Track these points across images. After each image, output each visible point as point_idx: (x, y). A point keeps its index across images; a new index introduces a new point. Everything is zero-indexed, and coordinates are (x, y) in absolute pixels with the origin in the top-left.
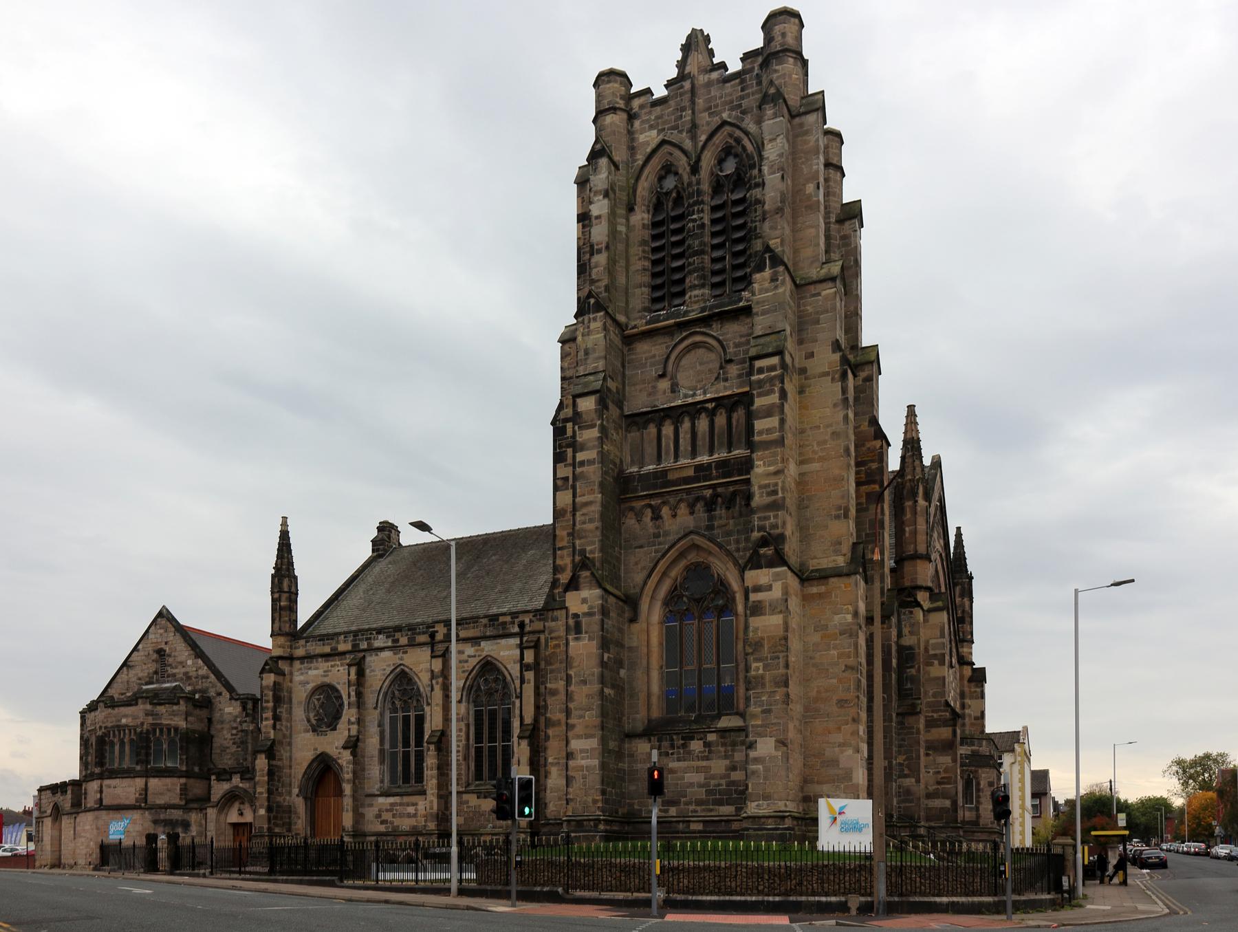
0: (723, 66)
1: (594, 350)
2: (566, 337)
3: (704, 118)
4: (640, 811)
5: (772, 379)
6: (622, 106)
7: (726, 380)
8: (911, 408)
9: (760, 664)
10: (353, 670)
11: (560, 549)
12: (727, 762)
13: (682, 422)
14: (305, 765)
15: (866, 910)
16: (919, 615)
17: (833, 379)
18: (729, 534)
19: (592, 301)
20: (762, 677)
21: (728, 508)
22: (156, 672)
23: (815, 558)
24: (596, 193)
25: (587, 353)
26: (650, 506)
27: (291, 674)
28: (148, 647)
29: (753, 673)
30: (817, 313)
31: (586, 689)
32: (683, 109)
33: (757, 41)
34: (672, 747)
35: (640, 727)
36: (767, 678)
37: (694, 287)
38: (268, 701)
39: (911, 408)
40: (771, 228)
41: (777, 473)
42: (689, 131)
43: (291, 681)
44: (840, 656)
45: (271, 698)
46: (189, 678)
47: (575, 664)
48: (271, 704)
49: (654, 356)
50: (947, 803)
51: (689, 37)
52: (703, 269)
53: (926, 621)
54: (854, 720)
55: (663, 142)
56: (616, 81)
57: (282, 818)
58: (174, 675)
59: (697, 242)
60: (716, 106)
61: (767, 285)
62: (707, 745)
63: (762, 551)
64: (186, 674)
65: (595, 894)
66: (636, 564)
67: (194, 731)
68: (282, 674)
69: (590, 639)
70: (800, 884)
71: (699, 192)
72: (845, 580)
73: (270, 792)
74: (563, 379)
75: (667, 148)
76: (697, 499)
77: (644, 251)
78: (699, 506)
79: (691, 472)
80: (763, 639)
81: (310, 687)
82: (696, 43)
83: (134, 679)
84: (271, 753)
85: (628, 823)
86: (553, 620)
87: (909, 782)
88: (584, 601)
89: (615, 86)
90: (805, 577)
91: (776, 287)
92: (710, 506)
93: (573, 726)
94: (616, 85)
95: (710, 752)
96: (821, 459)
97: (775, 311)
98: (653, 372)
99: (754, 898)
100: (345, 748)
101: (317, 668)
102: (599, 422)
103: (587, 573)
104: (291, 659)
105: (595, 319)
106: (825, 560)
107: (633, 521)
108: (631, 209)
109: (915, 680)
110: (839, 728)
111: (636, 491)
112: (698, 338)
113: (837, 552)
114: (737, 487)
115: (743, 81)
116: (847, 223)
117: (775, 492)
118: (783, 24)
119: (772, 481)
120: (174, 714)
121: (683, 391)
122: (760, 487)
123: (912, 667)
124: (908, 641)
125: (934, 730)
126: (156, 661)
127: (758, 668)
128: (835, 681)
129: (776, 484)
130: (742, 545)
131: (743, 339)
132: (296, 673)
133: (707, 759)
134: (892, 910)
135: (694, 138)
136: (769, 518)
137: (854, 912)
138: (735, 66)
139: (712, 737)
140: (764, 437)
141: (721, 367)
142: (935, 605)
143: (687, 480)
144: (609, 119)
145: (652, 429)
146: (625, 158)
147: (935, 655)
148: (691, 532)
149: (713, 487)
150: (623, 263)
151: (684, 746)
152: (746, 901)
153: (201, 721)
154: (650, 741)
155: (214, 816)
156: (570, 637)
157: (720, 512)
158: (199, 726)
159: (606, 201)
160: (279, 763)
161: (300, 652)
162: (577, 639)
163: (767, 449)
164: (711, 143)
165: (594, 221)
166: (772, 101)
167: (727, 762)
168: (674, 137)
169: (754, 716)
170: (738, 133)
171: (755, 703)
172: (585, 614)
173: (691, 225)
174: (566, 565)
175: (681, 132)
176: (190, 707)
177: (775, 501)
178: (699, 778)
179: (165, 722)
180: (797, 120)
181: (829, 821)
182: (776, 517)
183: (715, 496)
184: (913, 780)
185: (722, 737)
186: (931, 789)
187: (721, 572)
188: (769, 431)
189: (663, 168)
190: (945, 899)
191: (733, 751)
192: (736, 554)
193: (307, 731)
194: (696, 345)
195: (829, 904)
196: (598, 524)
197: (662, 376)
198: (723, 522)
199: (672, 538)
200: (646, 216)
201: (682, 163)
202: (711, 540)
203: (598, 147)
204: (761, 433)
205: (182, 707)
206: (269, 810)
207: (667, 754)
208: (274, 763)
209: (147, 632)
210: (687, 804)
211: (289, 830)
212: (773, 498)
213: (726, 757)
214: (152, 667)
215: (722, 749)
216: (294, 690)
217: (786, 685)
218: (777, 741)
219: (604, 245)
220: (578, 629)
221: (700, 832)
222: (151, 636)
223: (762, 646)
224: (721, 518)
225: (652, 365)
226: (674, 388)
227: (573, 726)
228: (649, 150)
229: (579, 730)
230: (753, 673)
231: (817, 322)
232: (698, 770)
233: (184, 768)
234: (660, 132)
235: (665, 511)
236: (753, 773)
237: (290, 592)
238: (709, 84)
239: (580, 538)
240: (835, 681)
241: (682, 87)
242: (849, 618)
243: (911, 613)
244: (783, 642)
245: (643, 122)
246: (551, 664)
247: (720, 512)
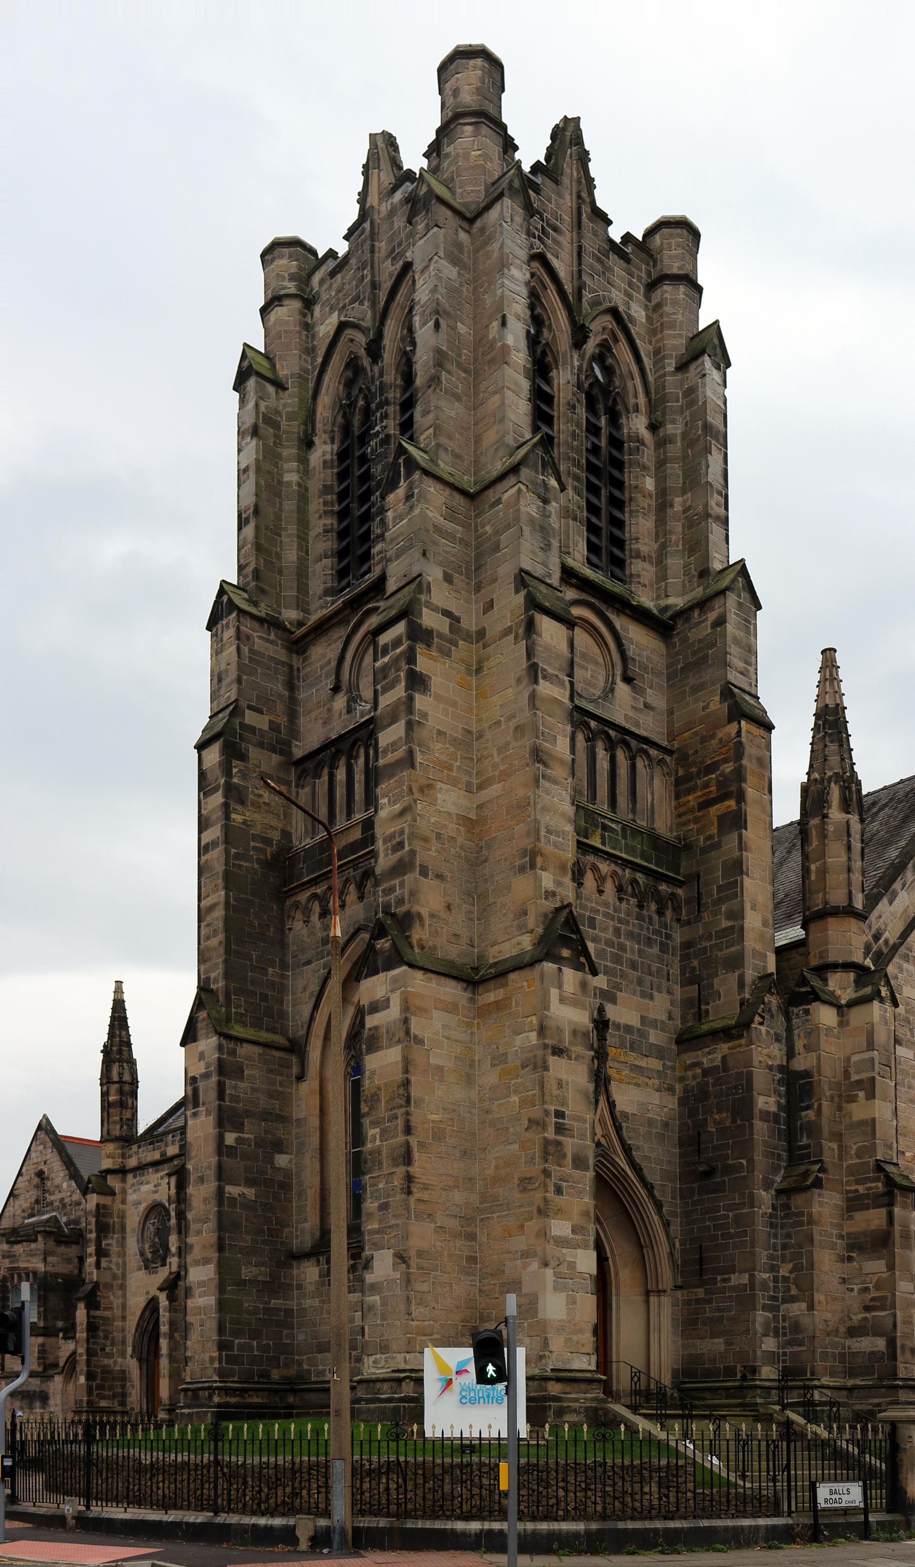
4: (309, 1371)
8: (829, 655)
10: (173, 1180)
14: (139, 1313)
15: (321, 1542)
16: (826, 1016)
17: (516, 638)
22: (37, 1201)
23: (495, 943)
26: (315, 896)
27: (124, 1192)
28: (30, 1170)
38: (91, 1232)
39: (829, 655)
43: (124, 1202)
44: (523, 1102)
45: (93, 1227)
46: (64, 1206)
48: (93, 1236)
50: (880, 1344)
53: (842, 1024)
54: (539, 1211)
55: (342, 326)
56: (281, 257)
57: (111, 1388)
58: (51, 1203)
64: (62, 1200)
66: (305, 989)
67: (56, 1275)
68: (112, 1193)
69: (208, 1114)
70: (295, 1494)
72: (526, 973)
73: (90, 1353)
77: (325, 503)
81: (142, 1207)
82: (384, 148)
83: (19, 1212)
84: (92, 1303)
85: (294, 1391)
87: (797, 1309)
90: (474, 977)
94: (283, 262)
100: (161, 1289)
101: (148, 1183)
104: (122, 1172)
106: (506, 946)
108: (308, 443)
109: (813, 1129)
110: (522, 1227)
111: (301, 875)
113: (523, 929)
116: (692, 367)
120: (32, 1254)
123: (808, 1107)
124: (801, 1063)
125: (858, 1215)
126: (36, 1187)
128: (515, 1147)
129: (402, 832)
132: (130, 1191)
134: (361, 1541)
137: (304, 1545)
142: (861, 993)
144: (279, 313)
146: (296, 369)
147: (860, 1082)
150: (292, 529)
153: (68, 1261)
155: (60, 1386)
158: (63, 1269)
160: (107, 1313)
161: (132, 1162)
164: (394, 306)
176: (51, 1244)
177: (401, 860)
179: (23, 1265)
180: (478, 224)
181: (439, 1386)
182: (402, 885)
184: (804, 1305)
186: (856, 1318)
189: (347, 366)
190: (474, 1526)
193: (140, 1269)
195: (269, 1529)
196: (221, 937)
197: (336, 689)
203: (246, 364)
205: (40, 1245)
206: (90, 1376)
208: (97, 1313)
209: (29, 1150)
211: (123, 1403)
214: (33, 1194)
216: (128, 1214)
222: (33, 1155)
223: (379, 1100)
225: (327, 677)
230: (369, 1146)
231: (497, 548)
233: (41, 1324)
237: (121, 1082)
240: (515, 1147)
242: (533, 1036)
243: (807, 1012)
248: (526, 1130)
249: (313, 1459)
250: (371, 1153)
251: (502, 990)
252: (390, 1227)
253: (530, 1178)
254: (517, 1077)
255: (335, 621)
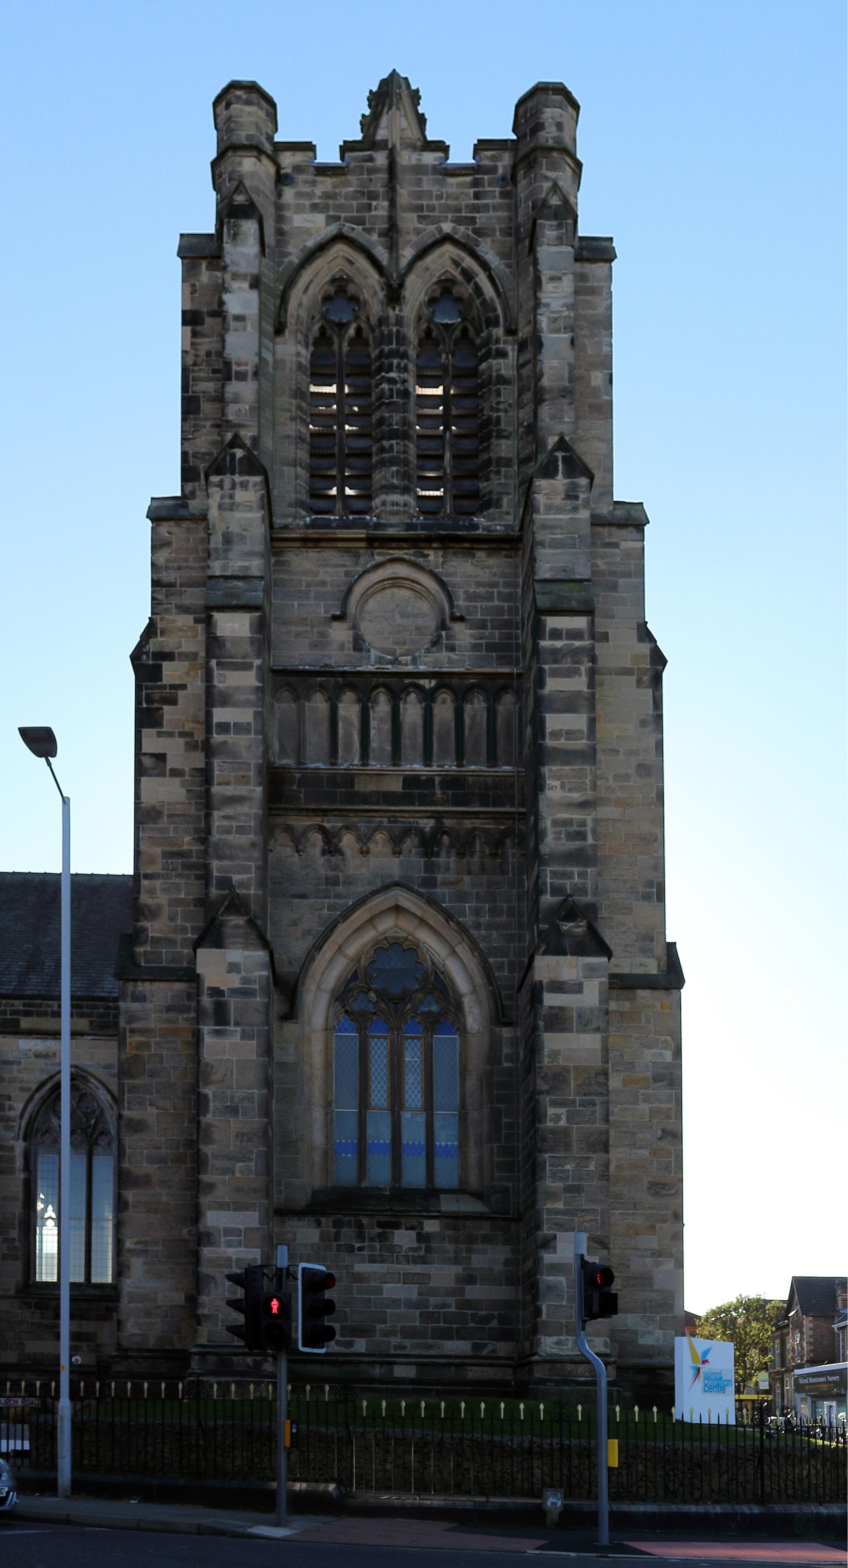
0: (441, 147)
1: (242, 539)
2: (164, 513)
3: (408, 221)
5: (575, 653)
6: (269, 152)
7: (452, 649)
9: (562, 1111)
11: (147, 876)
12: (458, 1269)
13: (376, 702)
17: (639, 682)
18: (462, 897)
19: (239, 453)
20: (566, 1132)
21: (461, 855)
24: (235, 276)
25: (228, 539)
26: (322, 830)
29: (550, 1124)
30: (613, 573)
31: (235, 1124)
32: (373, 196)
33: (503, 129)
34: (361, 1237)
35: (302, 1200)
36: (575, 1135)
37: (390, 488)
40: (553, 417)
41: (583, 805)
42: (384, 234)
44: (654, 1113)
47: (215, 1077)
49: (323, 583)
51: (384, 83)
52: (406, 462)
55: (339, 237)
56: (261, 108)
59: (396, 417)
60: (432, 208)
61: (558, 500)
62: (422, 1238)
63: (566, 926)
65: (411, 1500)
66: (295, 923)
69: (245, 1036)
71: (401, 339)
74: (155, 583)
75: (341, 249)
76: (407, 832)
77: (299, 408)
78: (409, 844)
79: (396, 786)
80: (566, 1070)
86: (136, 998)
88: (233, 968)
89: (248, 115)
91: (575, 509)
92: (429, 845)
93: (211, 1187)
95: (428, 1250)
96: (619, 803)
97: (574, 546)
98: (321, 611)
99: (718, 1509)
102: (257, 662)
103: (241, 921)
105: (244, 486)
107: (289, 850)
110: (653, 1227)
112: (402, 570)
114: (478, 823)
115: (476, 183)
117: (581, 836)
118: (545, 114)
119: (577, 816)
121: (374, 653)
122: (555, 823)
127: (558, 1118)
130: (485, 919)
131: (482, 590)
133: (424, 1261)
135: (393, 247)
136: (570, 876)
138: (461, 154)
139: (431, 1226)
140: (562, 743)
141: (443, 626)
143: (388, 798)
145: (319, 704)
148: (397, 884)
149: (438, 816)
151: (382, 1237)
152: (707, 1515)
154: (319, 1224)
156: (206, 1029)
157: (447, 860)
159: (254, 295)
162: (218, 1033)
163: (568, 763)
164: (420, 265)
165: (232, 324)
166: (556, 217)
167: (458, 1269)
168: (357, 232)
169: (552, 1196)
170: (469, 262)
171: (554, 1175)
172: (235, 992)
173: (385, 386)
174: (159, 907)
175: (369, 231)
178: (411, 1292)
183: (439, 830)
185: (455, 1228)
187: (437, 959)
188: (570, 735)
189: (333, 281)
191: (469, 1251)
192: (474, 932)
194: (395, 582)
198: (451, 876)
199: (360, 890)
200: (303, 351)
201: (370, 284)
202: (432, 902)
204: (556, 735)
207: (351, 1249)
210: (386, 1334)
212: (577, 844)
213: (456, 1261)
215: (450, 1247)
217: (606, 1149)
218: (591, 1239)
219: (250, 369)
220: (221, 1015)
221: (411, 1381)
223: (565, 1081)
224: (448, 870)
226: (358, 644)
227: (211, 1187)
228: (310, 243)
229: (222, 1193)
230: (550, 1124)
232: (408, 1279)
234: (331, 220)
235: (348, 841)
236: (551, 1288)
238: (419, 169)
239: (220, 858)
240: (645, 1153)
241: (371, 159)
244: (601, 1079)
245: (299, 195)
246: (131, 1076)
247: (447, 860)
248: (660, 1139)
249: (687, 1444)
250: (554, 1132)
251: (627, 1004)
252: (584, 1211)
253: (664, 1184)
254: (648, 1088)
255: (339, 545)
